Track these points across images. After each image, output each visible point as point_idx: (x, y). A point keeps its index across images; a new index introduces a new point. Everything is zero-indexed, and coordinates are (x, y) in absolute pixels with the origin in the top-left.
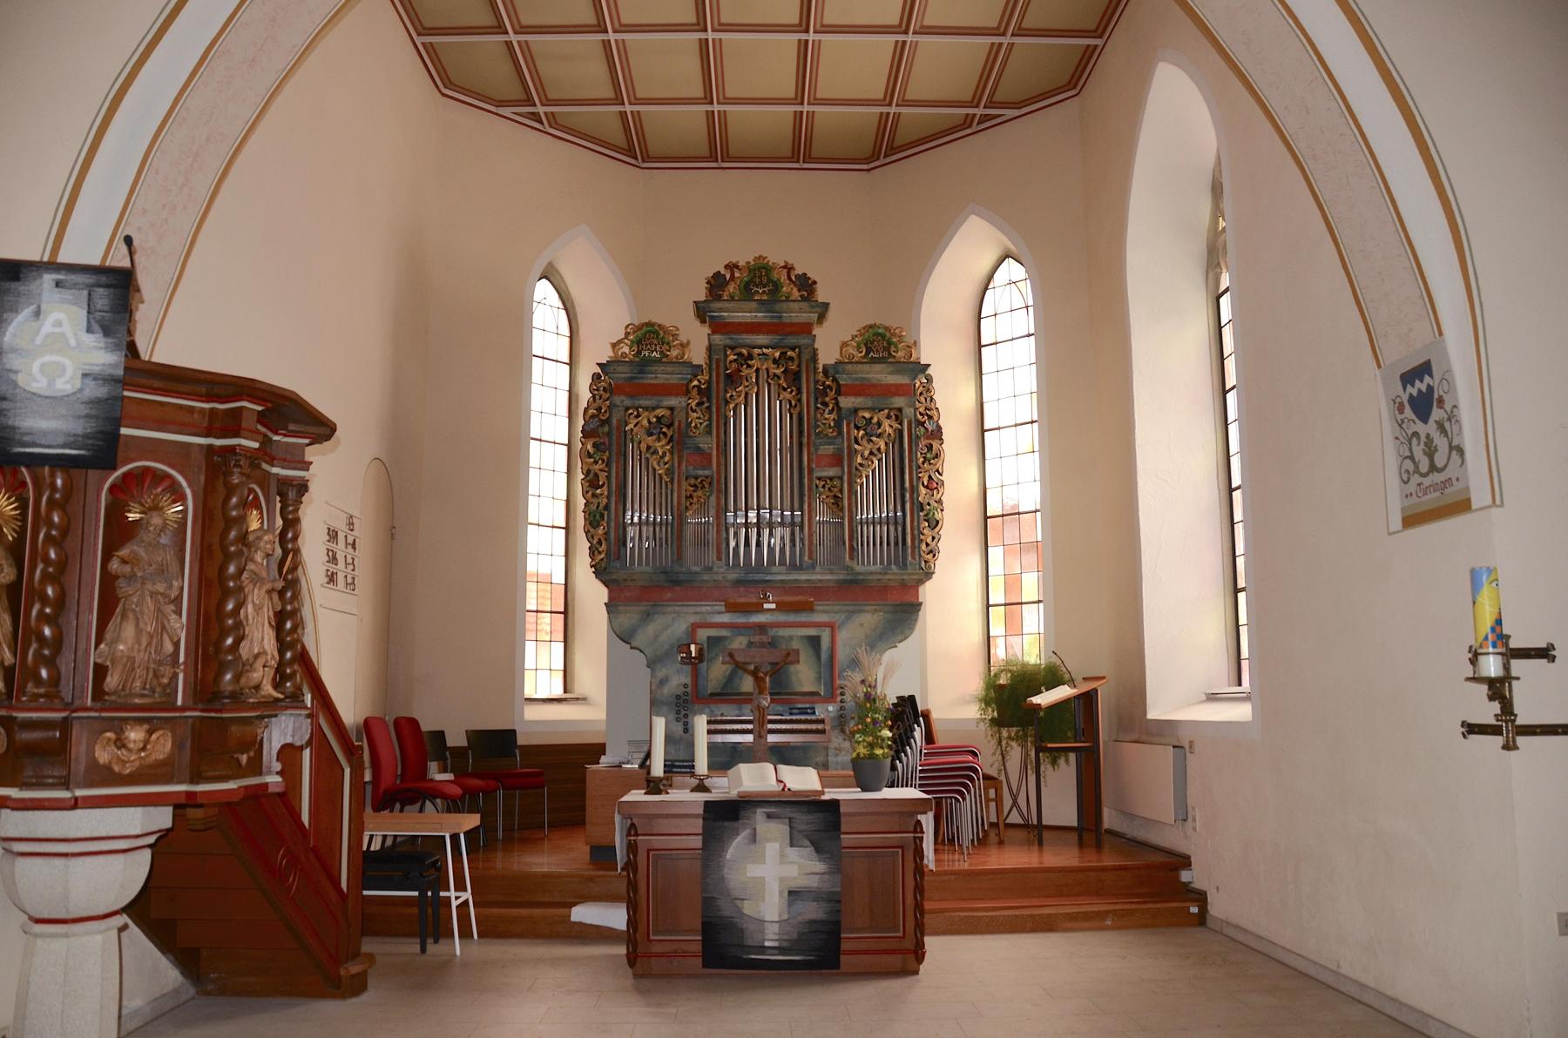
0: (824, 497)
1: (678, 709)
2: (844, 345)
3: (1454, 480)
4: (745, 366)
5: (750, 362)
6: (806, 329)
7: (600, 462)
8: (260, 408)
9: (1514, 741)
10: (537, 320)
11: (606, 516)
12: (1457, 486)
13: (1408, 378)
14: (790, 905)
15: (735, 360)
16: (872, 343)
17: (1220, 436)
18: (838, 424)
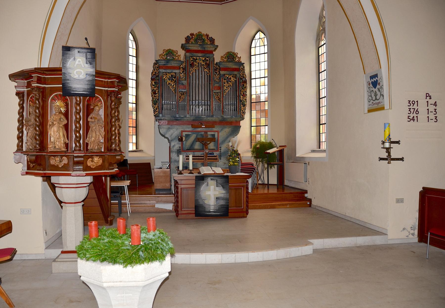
2: (222, 57)
3: (381, 102)
4: (195, 62)
5: (196, 61)
6: (211, 52)
7: (156, 87)
8: (118, 81)
9: (390, 162)
12: (381, 104)
13: (372, 77)
15: (192, 60)
17: (318, 85)
18: (220, 78)
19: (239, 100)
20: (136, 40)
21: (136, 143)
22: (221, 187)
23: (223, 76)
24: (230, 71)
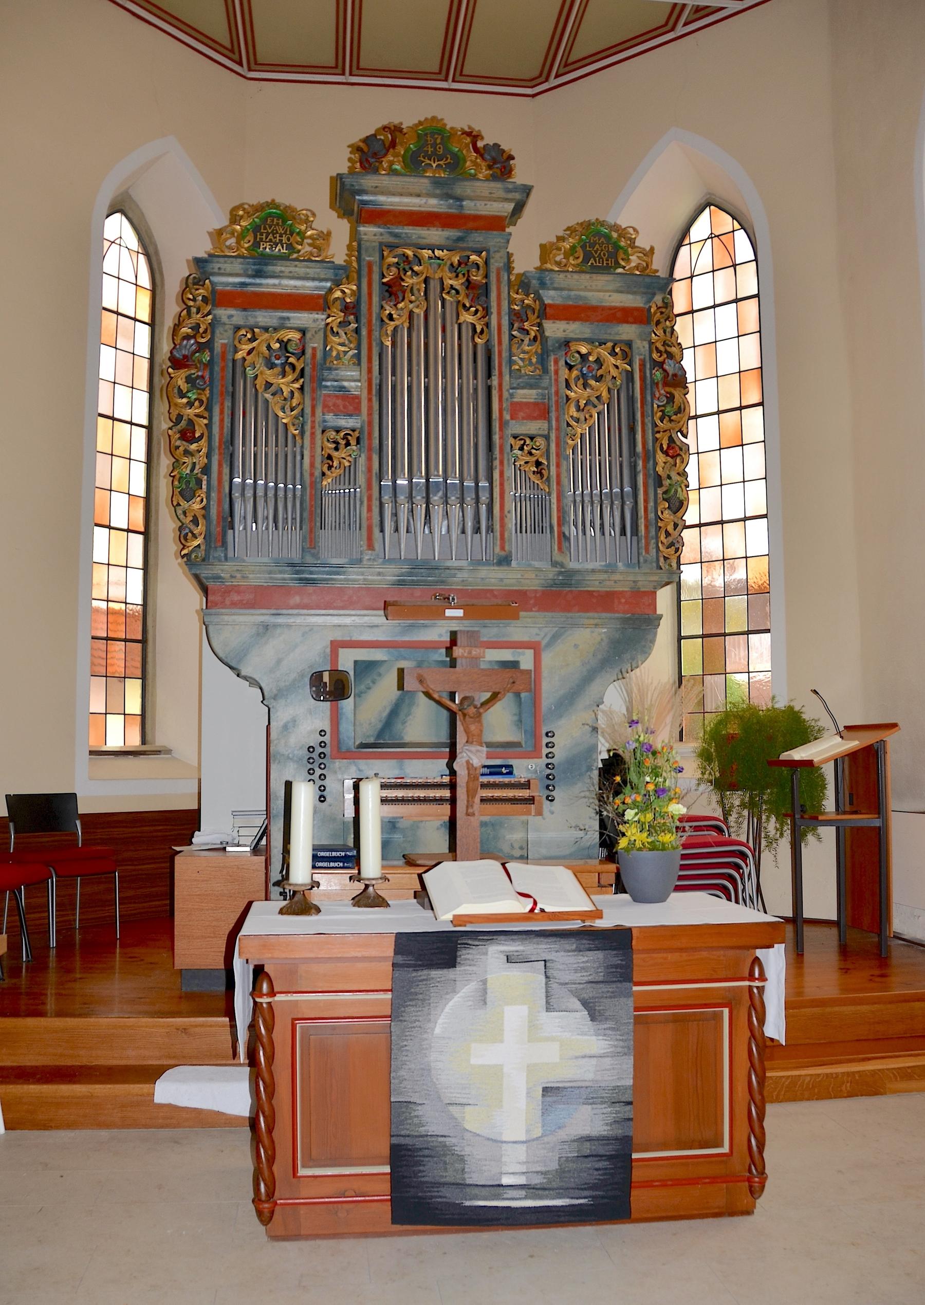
0: (522, 463)
1: (310, 766)
4: (409, 273)
7: (197, 404)
10: (109, 265)
11: (204, 483)
14: (545, 1112)
16: (592, 245)
19: (646, 476)
20: (151, 251)
21: (143, 715)
22: (578, 1015)
23: (560, 347)
24: (601, 321)
